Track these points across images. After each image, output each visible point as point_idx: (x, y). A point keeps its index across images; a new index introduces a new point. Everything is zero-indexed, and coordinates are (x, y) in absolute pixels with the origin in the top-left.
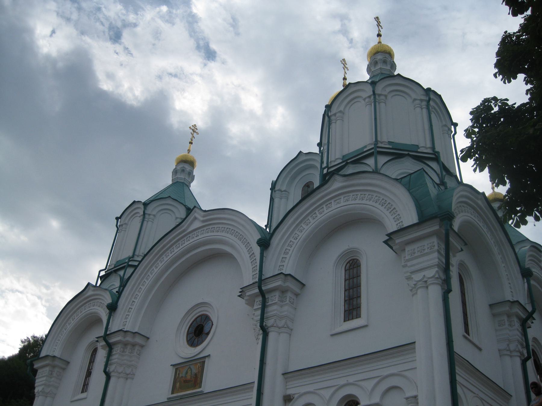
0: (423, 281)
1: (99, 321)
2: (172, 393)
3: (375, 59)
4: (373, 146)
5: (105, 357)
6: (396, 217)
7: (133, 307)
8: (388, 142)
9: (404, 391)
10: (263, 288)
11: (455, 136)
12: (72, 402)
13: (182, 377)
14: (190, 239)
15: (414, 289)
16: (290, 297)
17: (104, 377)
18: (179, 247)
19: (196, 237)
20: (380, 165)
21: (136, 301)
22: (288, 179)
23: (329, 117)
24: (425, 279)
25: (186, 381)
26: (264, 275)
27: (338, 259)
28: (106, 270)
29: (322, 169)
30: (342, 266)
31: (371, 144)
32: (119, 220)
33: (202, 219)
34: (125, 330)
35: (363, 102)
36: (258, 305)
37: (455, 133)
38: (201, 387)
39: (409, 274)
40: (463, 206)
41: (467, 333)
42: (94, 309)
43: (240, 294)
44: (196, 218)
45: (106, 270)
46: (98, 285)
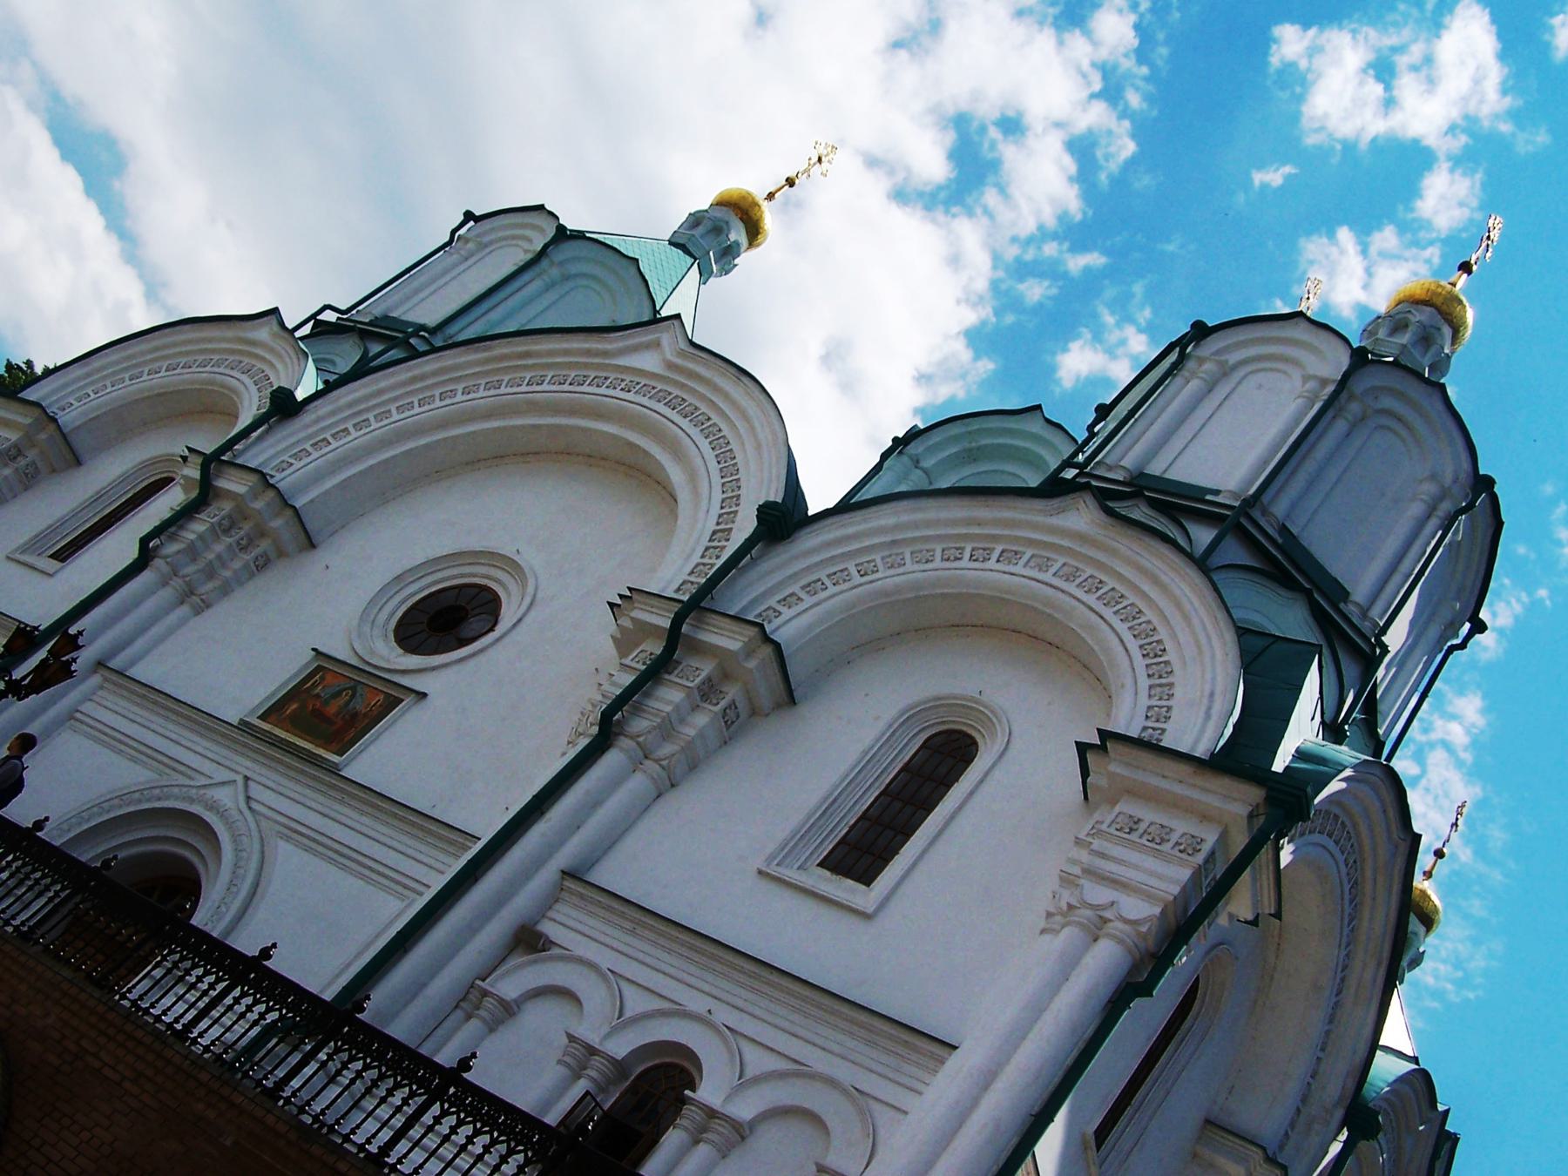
0: (1098, 913)
1: (234, 416)
2: (262, 717)
3: (1410, 316)
4: (1237, 504)
5: (172, 509)
6: (1156, 709)
7: (335, 444)
8: (1283, 525)
9: (828, 1133)
10: (685, 628)
11: (1455, 652)
12: (8, 558)
13: (318, 696)
14: (603, 384)
15: (1055, 919)
16: (734, 704)
17: (133, 553)
18: (560, 384)
19: (622, 389)
20: (1217, 560)
21: (354, 434)
22: (953, 450)
23: (1183, 357)
24: (1108, 914)
25: (318, 714)
26: (712, 598)
27: (930, 701)
28: (345, 317)
29: (1068, 463)
30: (920, 731)
31: (1234, 495)
32: (472, 223)
33: (669, 356)
34: (272, 481)
35: (1298, 381)
36: (638, 661)
37: (1463, 646)
38: (342, 755)
39: (1076, 870)
40: (1343, 823)
41: (1096, 1138)
42: (238, 380)
43: (619, 601)
44: (657, 345)
45: (345, 317)
46: (298, 334)
